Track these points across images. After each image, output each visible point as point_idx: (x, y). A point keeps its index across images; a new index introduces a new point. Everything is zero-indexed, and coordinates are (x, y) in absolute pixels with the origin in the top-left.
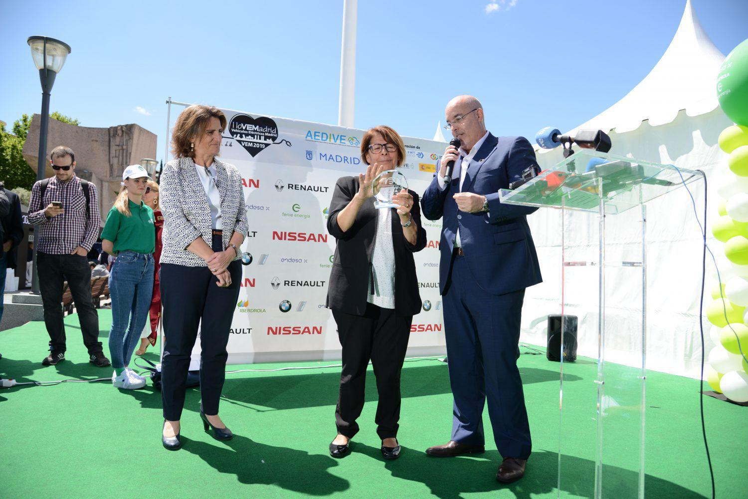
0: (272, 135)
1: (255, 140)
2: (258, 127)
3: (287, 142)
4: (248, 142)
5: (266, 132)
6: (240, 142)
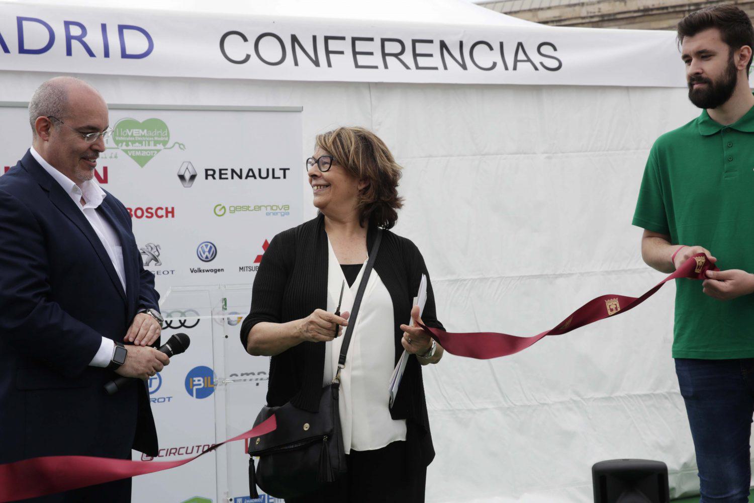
0: (162, 139)
1: (144, 148)
2: (145, 131)
3: (180, 145)
4: (135, 150)
5: (155, 136)
6: (126, 151)
